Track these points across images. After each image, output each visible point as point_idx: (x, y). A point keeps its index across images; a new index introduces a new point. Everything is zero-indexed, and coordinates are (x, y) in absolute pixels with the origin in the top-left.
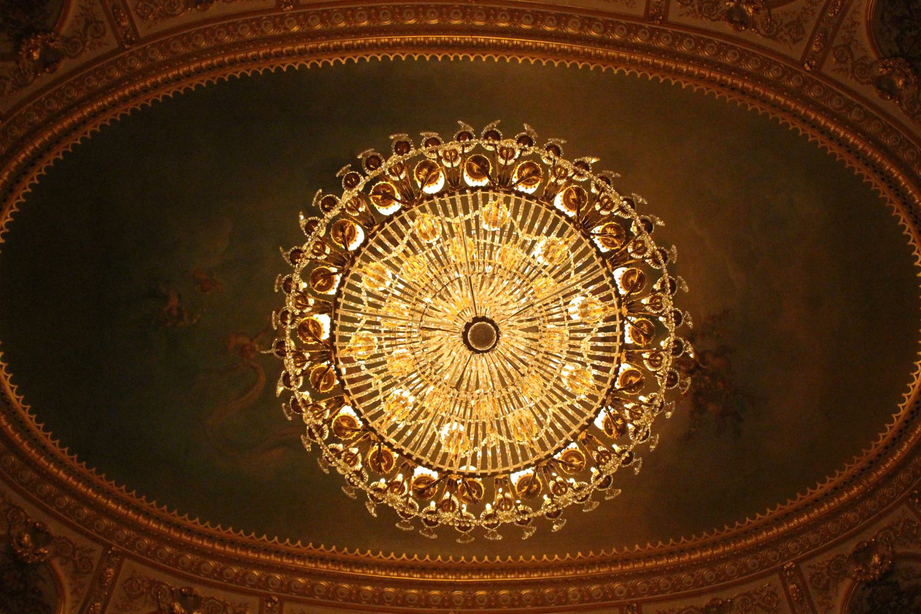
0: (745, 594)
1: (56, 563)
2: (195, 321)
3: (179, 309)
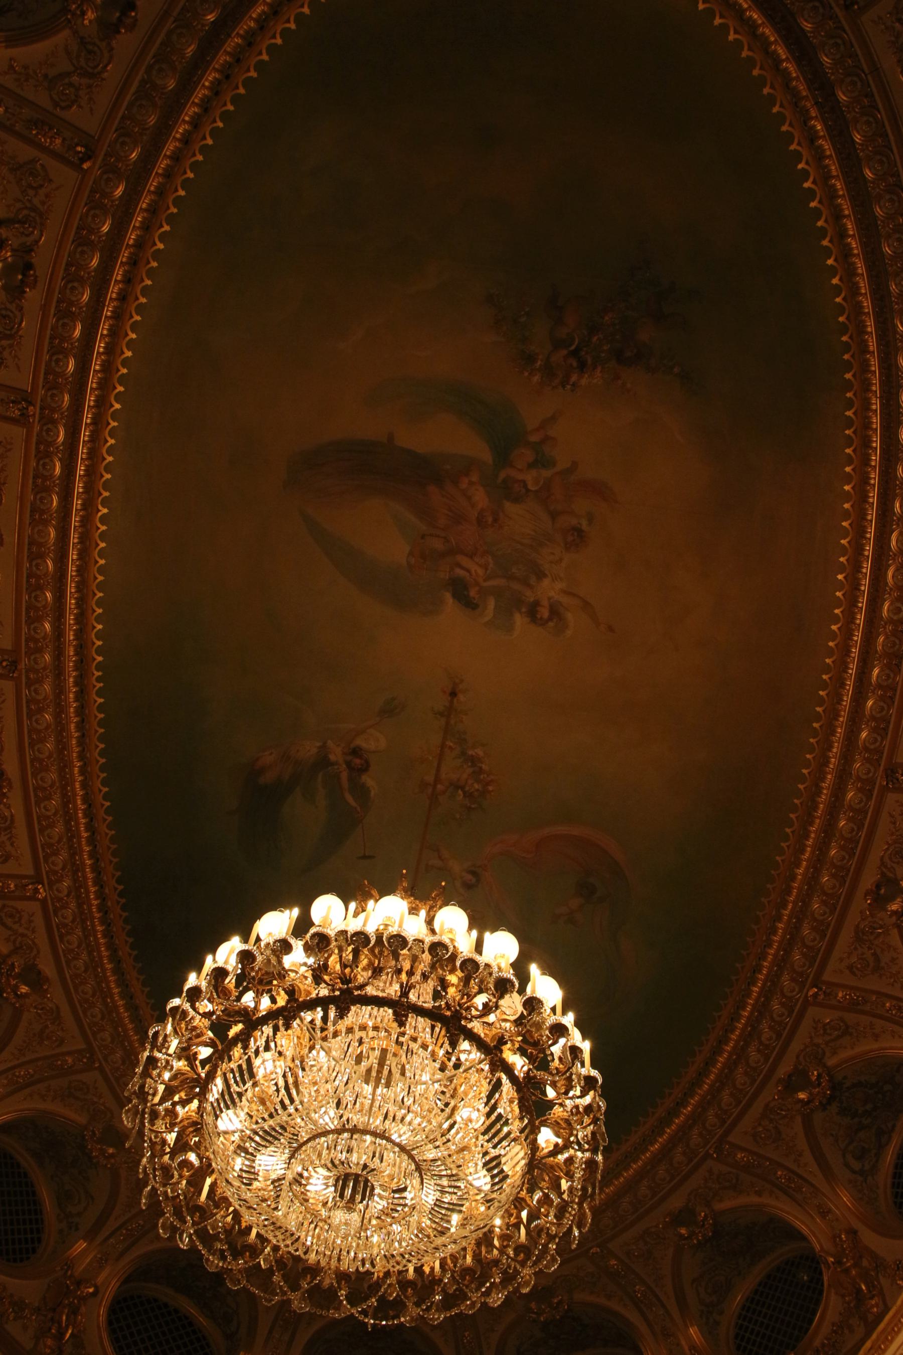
0: (12, 821)
1: (718, 1206)
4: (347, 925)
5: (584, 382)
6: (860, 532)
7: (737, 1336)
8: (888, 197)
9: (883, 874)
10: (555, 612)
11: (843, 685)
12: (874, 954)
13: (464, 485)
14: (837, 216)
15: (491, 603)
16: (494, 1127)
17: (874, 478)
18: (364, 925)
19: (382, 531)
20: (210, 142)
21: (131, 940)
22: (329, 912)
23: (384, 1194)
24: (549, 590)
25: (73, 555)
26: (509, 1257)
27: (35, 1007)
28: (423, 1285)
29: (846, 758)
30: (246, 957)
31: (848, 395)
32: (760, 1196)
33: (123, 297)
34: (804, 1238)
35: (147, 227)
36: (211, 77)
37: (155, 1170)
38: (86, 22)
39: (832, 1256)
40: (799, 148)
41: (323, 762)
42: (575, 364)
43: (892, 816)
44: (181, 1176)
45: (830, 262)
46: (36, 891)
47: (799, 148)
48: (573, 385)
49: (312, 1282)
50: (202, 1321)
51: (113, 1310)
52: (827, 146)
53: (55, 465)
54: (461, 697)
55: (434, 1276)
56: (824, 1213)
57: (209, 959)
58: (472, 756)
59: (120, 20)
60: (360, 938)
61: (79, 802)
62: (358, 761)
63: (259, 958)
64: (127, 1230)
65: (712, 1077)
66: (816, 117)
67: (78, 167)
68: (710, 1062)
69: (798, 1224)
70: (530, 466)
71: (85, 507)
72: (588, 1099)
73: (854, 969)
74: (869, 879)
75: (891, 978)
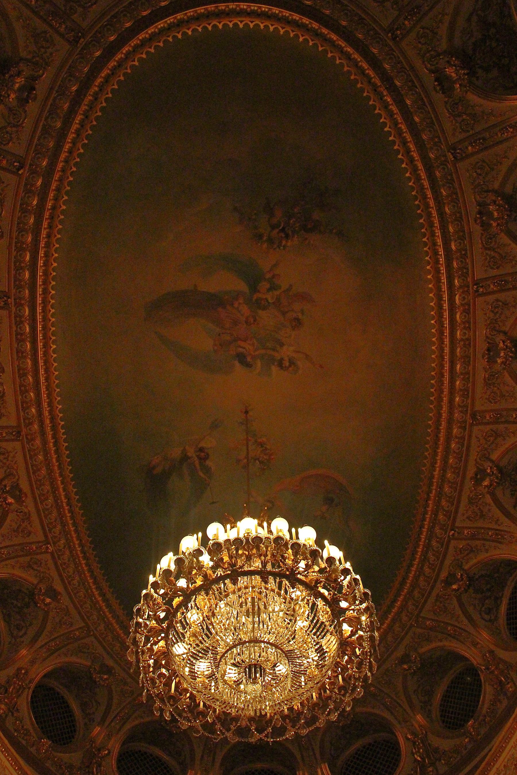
4: (228, 536)
5: (289, 244)
6: (440, 298)
7: (441, 716)
8: (428, 129)
9: (477, 467)
10: (292, 363)
11: (443, 376)
12: (480, 509)
13: (236, 305)
14: (405, 143)
15: (259, 363)
16: (318, 628)
17: (443, 270)
18: (238, 535)
19: (198, 334)
20: (82, 151)
21: (99, 566)
22: (216, 531)
24: (287, 352)
25: (42, 372)
26: (335, 692)
27: (55, 609)
28: (293, 717)
29: (451, 412)
30: (179, 562)
31: (423, 230)
33: (49, 236)
34: (467, 659)
35: (56, 199)
36: (79, 118)
37: (147, 680)
38: (11, 100)
39: (483, 666)
40: (380, 112)
41: (185, 458)
43: (477, 438)
44: (161, 682)
45: (403, 166)
46: (47, 548)
47: (380, 112)
48: (284, 246)
49: (236, 725)
50: (165, 757)
51: (119, 761)
52: (394, 108)
53: (26, 327)
54: (251, 413)
55: (299, 711)
56: (475, 644)
57: (158, 567)
58: (261, 442)
59: (28, 96)
60: (238, 541)
61: (63, 498)
62: (203, 454)
63: (186, 561)
64: (120, 717)
65: (408, 585)
66: (387, 95)
67: (16, 173)
68: (405, 579)
69: (463, 653)
70: (269, 290)
71: (44, 346)
72: (364, 605)
73: (471, 519)
74: (471, 471)
75: (490, 519)
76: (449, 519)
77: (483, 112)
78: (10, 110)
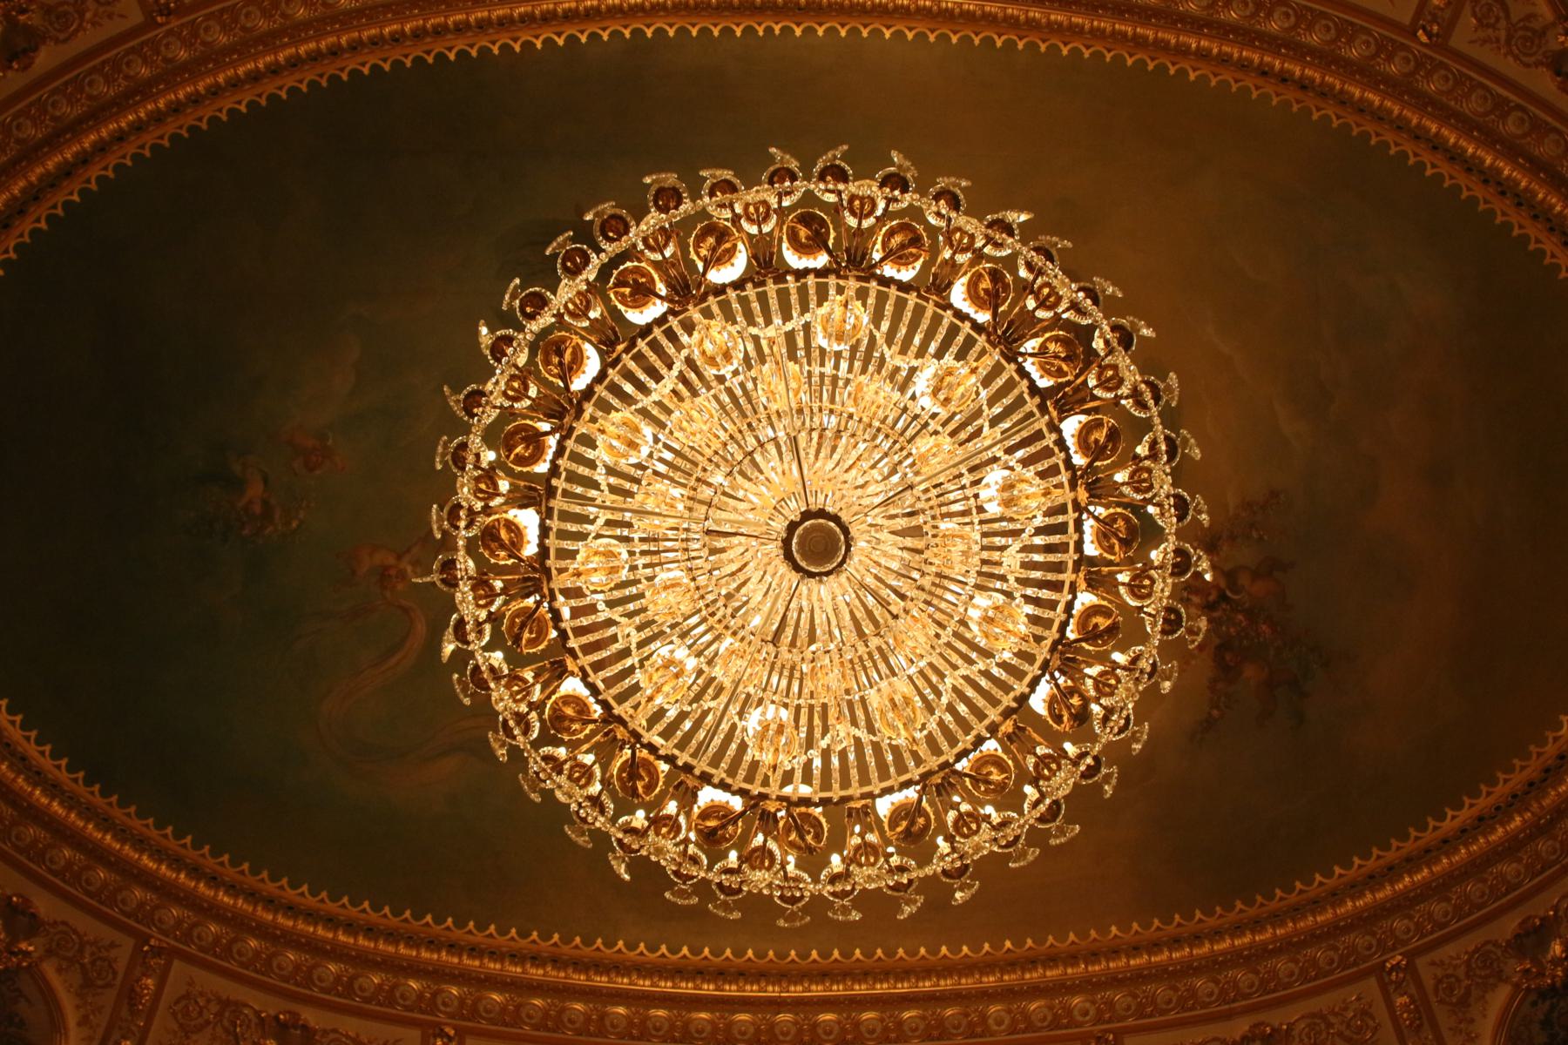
0: (1313, 1015)
1: (49, 969)
2: (294, 525)
3: (265, 503)
23: (803, 809)
32: (79, 1024)
42: (1211, 598)
76: (367, 1000)
77: (1472, 1021)
78: (1542, 33)
